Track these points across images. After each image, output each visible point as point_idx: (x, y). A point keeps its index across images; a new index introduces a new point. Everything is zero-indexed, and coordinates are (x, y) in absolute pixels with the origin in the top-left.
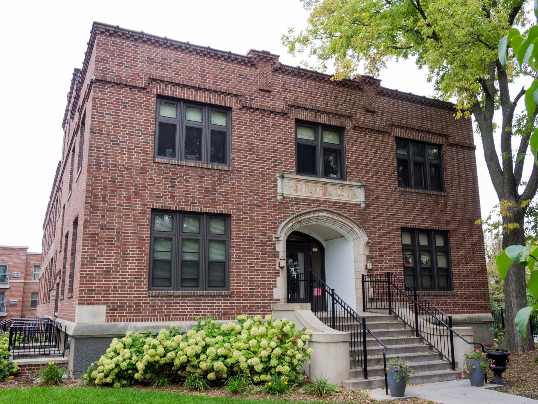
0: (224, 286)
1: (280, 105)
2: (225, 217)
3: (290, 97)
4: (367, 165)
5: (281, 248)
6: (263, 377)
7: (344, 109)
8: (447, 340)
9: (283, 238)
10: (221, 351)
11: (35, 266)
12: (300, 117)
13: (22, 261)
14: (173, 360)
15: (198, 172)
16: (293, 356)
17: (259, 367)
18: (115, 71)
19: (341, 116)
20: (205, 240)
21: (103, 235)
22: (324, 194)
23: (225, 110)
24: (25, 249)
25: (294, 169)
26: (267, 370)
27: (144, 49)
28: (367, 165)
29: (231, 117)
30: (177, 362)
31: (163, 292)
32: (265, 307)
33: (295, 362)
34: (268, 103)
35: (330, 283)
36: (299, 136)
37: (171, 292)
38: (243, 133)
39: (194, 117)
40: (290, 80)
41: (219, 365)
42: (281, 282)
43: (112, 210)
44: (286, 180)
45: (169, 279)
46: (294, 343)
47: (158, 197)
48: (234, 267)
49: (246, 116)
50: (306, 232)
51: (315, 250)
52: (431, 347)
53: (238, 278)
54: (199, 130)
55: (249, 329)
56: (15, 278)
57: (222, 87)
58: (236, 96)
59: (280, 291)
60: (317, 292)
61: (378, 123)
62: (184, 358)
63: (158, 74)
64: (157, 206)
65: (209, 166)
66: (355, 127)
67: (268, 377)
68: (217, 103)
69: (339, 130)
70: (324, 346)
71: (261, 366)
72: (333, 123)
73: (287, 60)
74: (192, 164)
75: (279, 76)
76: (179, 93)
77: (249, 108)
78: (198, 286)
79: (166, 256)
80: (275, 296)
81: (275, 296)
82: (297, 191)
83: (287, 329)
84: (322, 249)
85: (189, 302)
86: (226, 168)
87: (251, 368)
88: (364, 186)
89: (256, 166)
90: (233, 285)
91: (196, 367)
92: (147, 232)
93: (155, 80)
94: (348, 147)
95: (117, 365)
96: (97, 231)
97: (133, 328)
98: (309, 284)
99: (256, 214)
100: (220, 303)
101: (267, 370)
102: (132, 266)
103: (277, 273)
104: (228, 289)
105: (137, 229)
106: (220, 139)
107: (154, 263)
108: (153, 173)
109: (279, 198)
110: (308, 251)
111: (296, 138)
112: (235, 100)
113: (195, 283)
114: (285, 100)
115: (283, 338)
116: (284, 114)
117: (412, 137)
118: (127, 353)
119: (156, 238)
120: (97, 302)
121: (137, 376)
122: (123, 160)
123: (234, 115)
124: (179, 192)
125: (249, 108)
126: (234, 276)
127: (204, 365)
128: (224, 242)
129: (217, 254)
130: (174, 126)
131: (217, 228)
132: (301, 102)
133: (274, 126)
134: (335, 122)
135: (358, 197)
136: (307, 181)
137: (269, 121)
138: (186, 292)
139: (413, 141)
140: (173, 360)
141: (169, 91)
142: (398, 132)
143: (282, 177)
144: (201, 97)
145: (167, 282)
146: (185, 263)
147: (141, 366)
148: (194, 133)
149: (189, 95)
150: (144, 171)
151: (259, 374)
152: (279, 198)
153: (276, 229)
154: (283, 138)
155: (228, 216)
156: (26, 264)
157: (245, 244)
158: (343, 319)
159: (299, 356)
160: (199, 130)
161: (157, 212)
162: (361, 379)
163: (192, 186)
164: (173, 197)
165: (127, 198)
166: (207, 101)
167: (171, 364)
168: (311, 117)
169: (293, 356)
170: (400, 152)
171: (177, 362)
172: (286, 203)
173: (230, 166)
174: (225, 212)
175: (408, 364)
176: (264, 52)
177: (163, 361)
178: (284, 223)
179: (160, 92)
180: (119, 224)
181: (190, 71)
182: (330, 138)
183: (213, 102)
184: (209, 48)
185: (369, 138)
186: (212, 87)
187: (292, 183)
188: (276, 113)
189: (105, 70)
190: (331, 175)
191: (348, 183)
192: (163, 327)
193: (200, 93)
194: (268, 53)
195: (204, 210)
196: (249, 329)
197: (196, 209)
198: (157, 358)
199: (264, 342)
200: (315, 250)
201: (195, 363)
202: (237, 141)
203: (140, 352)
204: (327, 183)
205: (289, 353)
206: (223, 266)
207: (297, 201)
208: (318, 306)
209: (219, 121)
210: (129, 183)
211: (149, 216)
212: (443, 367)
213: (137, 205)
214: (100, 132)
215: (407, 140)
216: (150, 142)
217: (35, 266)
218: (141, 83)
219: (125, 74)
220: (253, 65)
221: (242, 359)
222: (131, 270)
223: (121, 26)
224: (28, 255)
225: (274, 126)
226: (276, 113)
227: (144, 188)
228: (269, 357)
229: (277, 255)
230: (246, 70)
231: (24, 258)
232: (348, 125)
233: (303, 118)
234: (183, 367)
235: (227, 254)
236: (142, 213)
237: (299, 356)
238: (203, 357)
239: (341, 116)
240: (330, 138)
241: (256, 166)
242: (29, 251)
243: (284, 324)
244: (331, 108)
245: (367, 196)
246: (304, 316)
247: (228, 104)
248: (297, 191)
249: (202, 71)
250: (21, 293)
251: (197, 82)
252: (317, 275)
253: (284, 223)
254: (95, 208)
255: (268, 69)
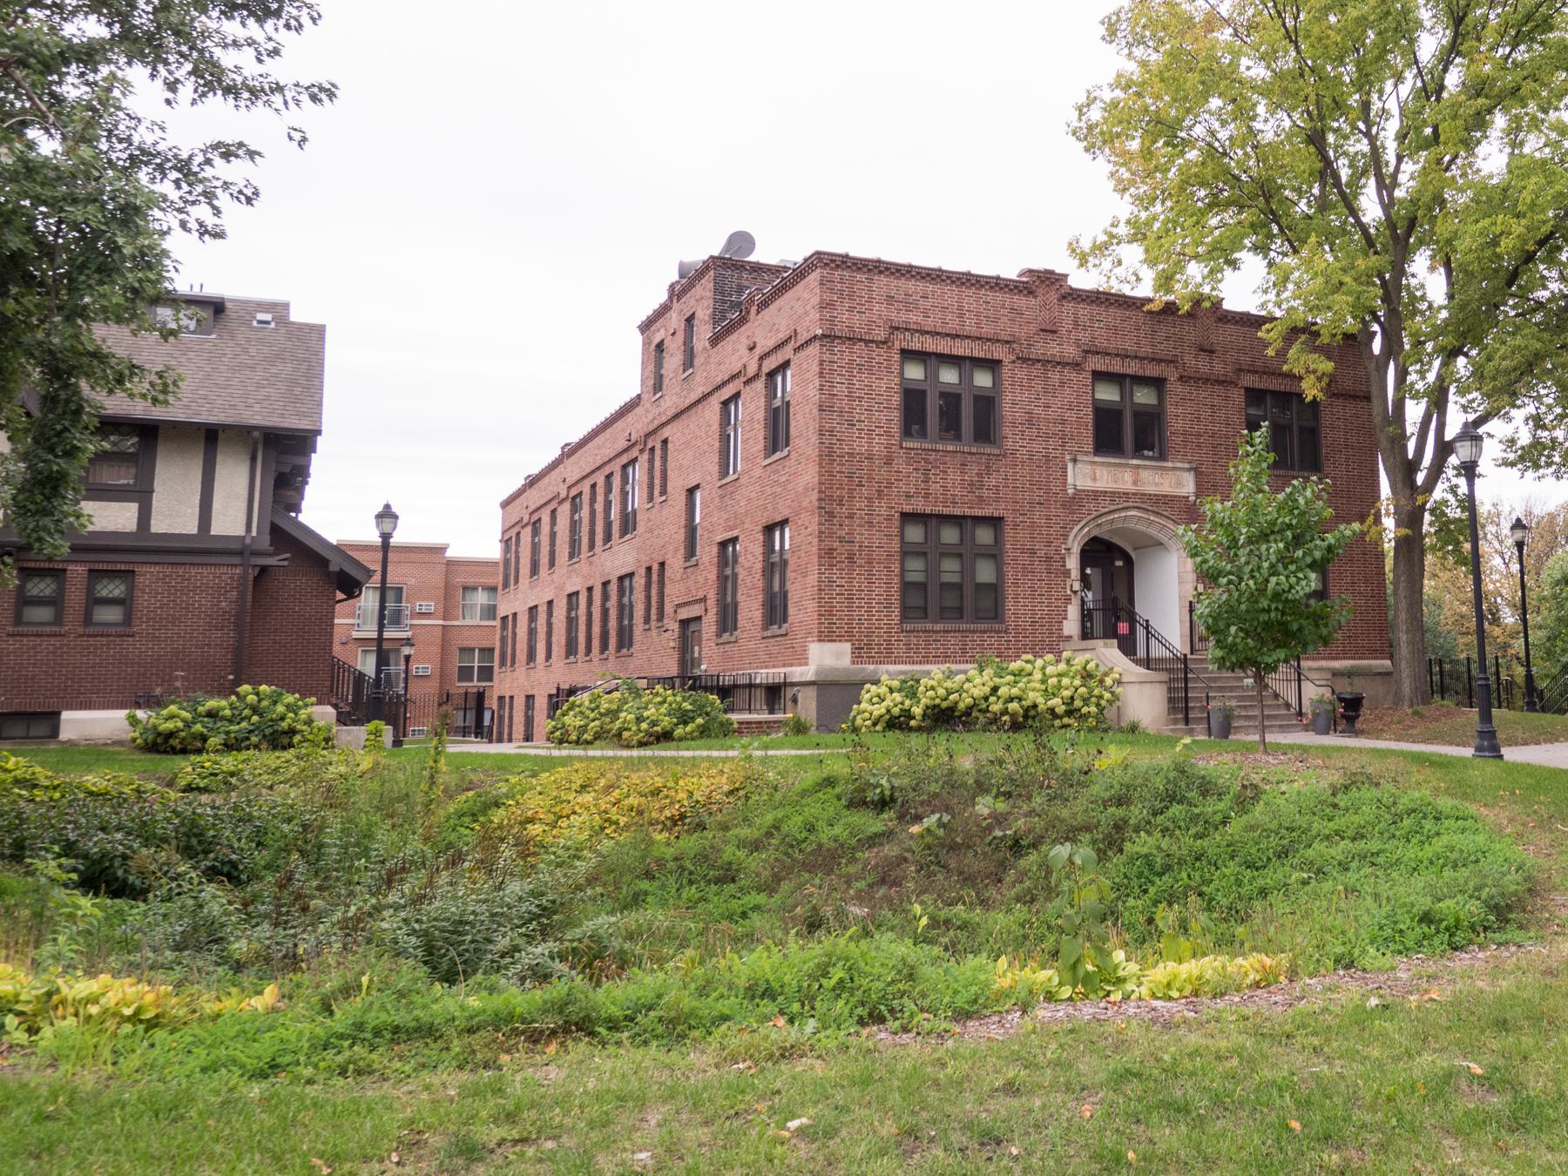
0: (996, 617)
1: (1071, 352)
2: (995, 522)
3: (1084, 337)
4: (1199, 435)
5: (1073, 563)
6: (1066, 720)
7: (1164, 349)
8: (1294, 685)
9: (1076, 549)
10: (1015, 691)
11: (465, 588)
12: (1101, 367)
13: (436, 577)
14: (956, 703)
15: (959, 458)
16: (1101, 697)
17: (1061, 709)
18: (846, 319)
19: (1160, 361)
20: (966, 554)
21: (842, 550)
22: (1135, 483)
23: (993, 365)
24: (441, 550)
25: (1090, 448)
26: (1069, 713)
27: (881, 281)
28: (1199, 435)
29: (1000, 374)
30: (962, 706)
31: (919, 626)
32: (1052, 644)
33: (1103, 703)
34: (1054, 349)
35: (1142, 609)
36: (1098, 396)
37: (929, 626)
38: (1018, 399)
39: (949, 376)
40: (1084, 310)
41: (1013, 706)
42: (1073, 611)
43: (851, 516)
44: (1079, 465)
45: (925, 609)
46: (1101, 681)
47: (908, 496)
48: (1010, 592)
49: (1021, 373)
50: (1106, 537)
51: (1119, 563)
52: (1276, 696)
53: (1016, 606)
54: (958, 397)
55: (1044, 668)
56: (422, 615)
57: (987, 330)
58: (1007, 342)
59: (1071, 626)
60: (1123, 628)
61: (1219, 369)
62: (969, 701)
63: (900, 318)
64: (907, 509)
65: (974, 450)
66: (1181, 378)
67: (1071, 721)
68: (982, 355)
69: (1158, 383)
70: (1137, 687)
71: (1064, 707)
72: (1148, 373)
73: (1082, 279)
74: (950, 448)
75: (1069, 306)
76: (931, 345)
77: (1024, 360)
78: (961, 617)
79: (955, 579)
80: (1066, 632)
81: (1066, 632)
82: (1095, 479)
83: (1091, 666)
84: (1129, 562)
85: (953, 640)
86: (996, 451)
87: (1052, 710)
88: (1195, 469)
89: (1037, 447)
90: (1011, 620)
91: (987, 711)
92: (896, 545)
93: (897, 329)
94: (1170, 410)
95: (888, 711)
96: (835, 545)
97: (890, 673)
98: (1114, 615)
99: (1038, 516)
100: (993, 640)
101: (1069, 713)
102: (879, 591)
103: (1068, 600)
104: (1002, 622)
105: (881, 540)
106: (987, 405)
107: (906, 586)
108: (900, 464)
109: (1070, 491)
110: (1112, 564)
111: (1094, 399)
112: (1006, 348)
113: (959, 613)
114: (1077, 344)
115: (1087, 676)
116: (1076, 366)
117: (1271, 387)
118: (897, 697)
119: (907, 552)
120: (840, 638)
121: (913, 723)
122: (861, 446)
123: (1006, 372)
124: (935, 488)
125: (1024, 360)
126: (1010, 604)
127: (996, 708)
128: (994, 556)
129: (985, 573)
130: (924, 393)
131: (984, 536)
132: (1102, 343)
133: (1062, 384)
134: (1152, 371)
135: (1186, 485)
136: (1109, 464)
137: (1055, 376)
138: (949, 626)
139: (1274, 393)
140: (956, 703)
141: (916, 345)
142: (1249, 381)
143: (1075, 461)
144: (960, 348)
145: (923, 613)
146: (944, 586)
147: (917, 711)
148: (951, 400)
149: (943, 346)
150: (889, 461)
151: (1061, 717)
152: (1070, 491)
153: (1066, 536)
154: (1074, 401)
155: (1000, 519)
156: (446, 583)
157: (1024, 559)
158: (1160, 660)
159: (1107, 695)
160: (958, 397)
161: (907, 518)
162: (1181, 726)
163: (950, 480)
164: (927, 496)
165: (870, 499)
166: (968, 353)
167: (952, 709)
168: (1116, 366)
169: (1101, 697)
170: (1252, 411)
171: (962, 706)
172: (1080, 499)
173: (1000, 447)
174: (996, 514)
175: (1234, 703)
176: (1047, 272)
177: (944, 705)
178: (1077, 528)
179: (904, 345)
180: (861, 535)
181: (940, 310)
182: (1144, 397)
183: (976, 354)
184: (969, 274)
185: (1204, 393)
186: (974, 331)
187: (1087, 469)
188: (1064, 364)
189: (832, 320)
190: (1146, 452)
191: (1170, 464)
192: (937, 670)
193: (958, 342)
194: (1052, 272)
195: (968, 512)
196: (1044, 668)
197: (958, 512)
198: (938, 701)
199: (1065, 681)
200: (1119, 563)
201: (984, 706)
202: (1012, 406)
203: (913, 694)
204: (1138, 467)
205: (1096, 692)
206: (995, 590)
207: (1096, 495)
208: (1128, 647)
209: (983, 380)
210: (870, 479)
211: (897, 523)
212: (1288, 717)
213: (881, 508)
214: (831, 409)
215: (1264, 392)
216: (892, 418)
217: (465, 588)
218: (881, 334)
219: (858, 322)
220: (1031, 293)
221: (1040, 700)
222: (878, 595)
223: (852, 254)
224: (451, 563)
225: (1062, 384)
226: (1064, 364)
227: (890, 485)
228: (1072, 698)
229: (1067, 573)
230: (1021, 301)
231: (442, 568)
232: (1171, 374)
233: (1104, 368)
234: (970, 709)
235: (1000, 574)
236: (889, 519)
237: (1107, 695)
238: (992, 699)
239: (1160, 361)
240: (1144, 397)
241: (1037, 447)
242: (449, 554)
243: (1088, 662)
244: (1146, 350)
245: (1198, 485)
246: (1108, 654)
247: (996, 356)
248: (1095, 479)
249: (960, 308)
250: (436, 650)
251: (953, 325)
252: (1123, 601)
253: (1077, 528)
254: (831, 514)
255: (1053, 296)
